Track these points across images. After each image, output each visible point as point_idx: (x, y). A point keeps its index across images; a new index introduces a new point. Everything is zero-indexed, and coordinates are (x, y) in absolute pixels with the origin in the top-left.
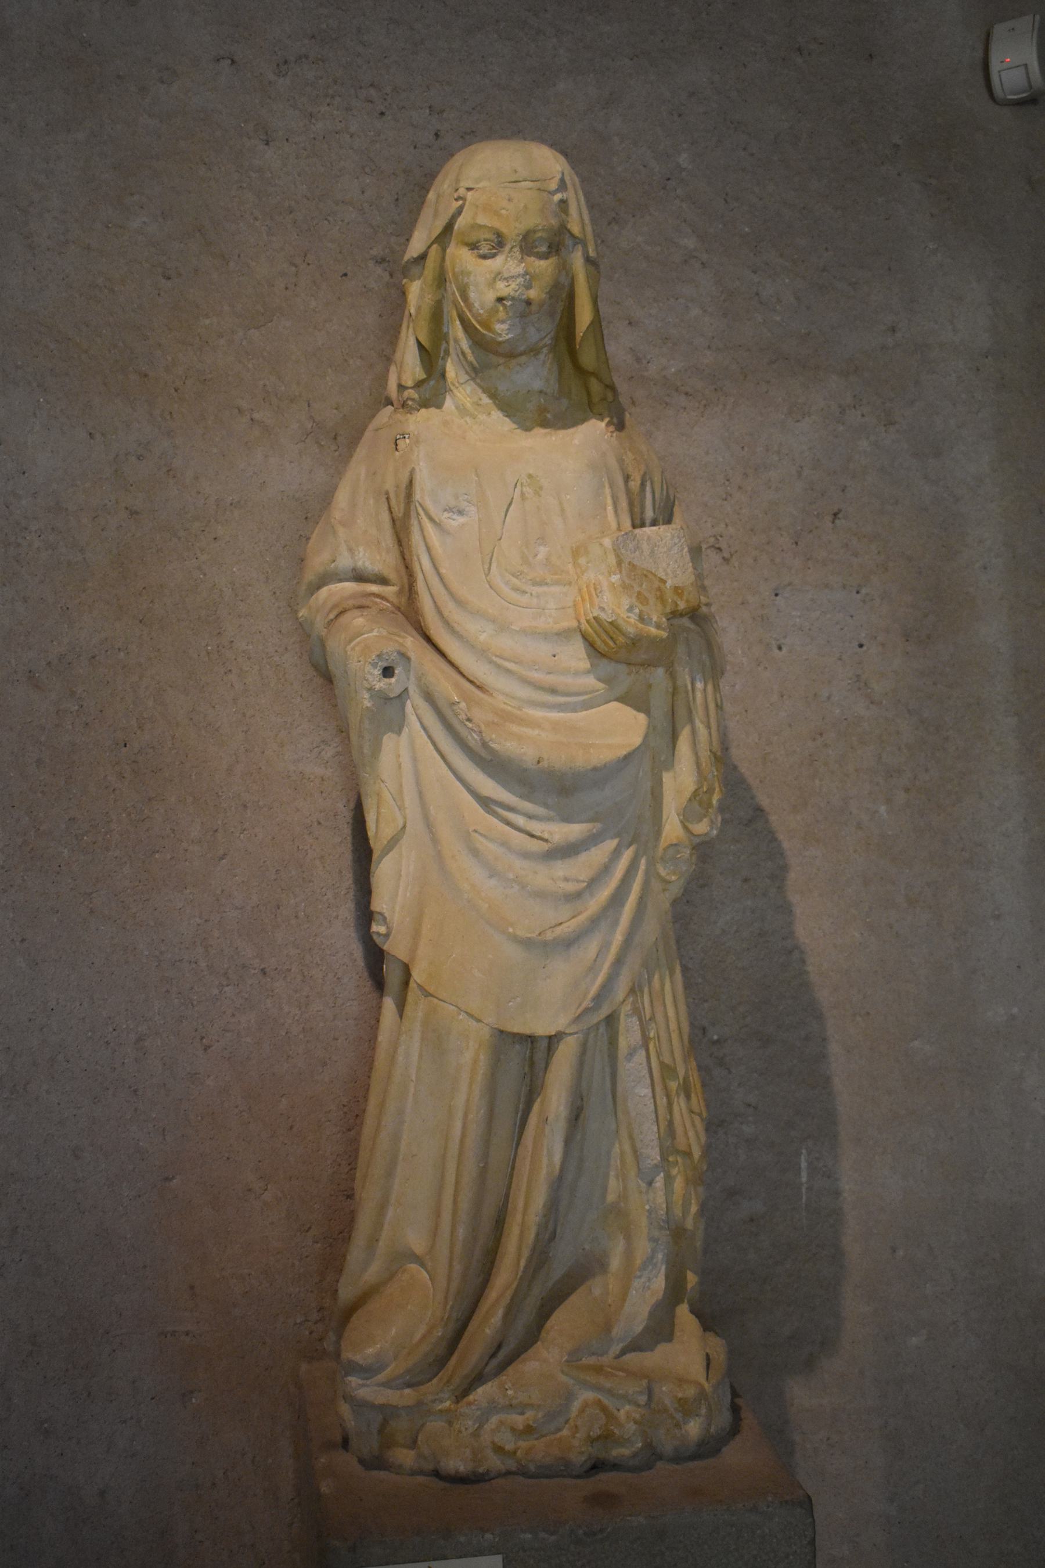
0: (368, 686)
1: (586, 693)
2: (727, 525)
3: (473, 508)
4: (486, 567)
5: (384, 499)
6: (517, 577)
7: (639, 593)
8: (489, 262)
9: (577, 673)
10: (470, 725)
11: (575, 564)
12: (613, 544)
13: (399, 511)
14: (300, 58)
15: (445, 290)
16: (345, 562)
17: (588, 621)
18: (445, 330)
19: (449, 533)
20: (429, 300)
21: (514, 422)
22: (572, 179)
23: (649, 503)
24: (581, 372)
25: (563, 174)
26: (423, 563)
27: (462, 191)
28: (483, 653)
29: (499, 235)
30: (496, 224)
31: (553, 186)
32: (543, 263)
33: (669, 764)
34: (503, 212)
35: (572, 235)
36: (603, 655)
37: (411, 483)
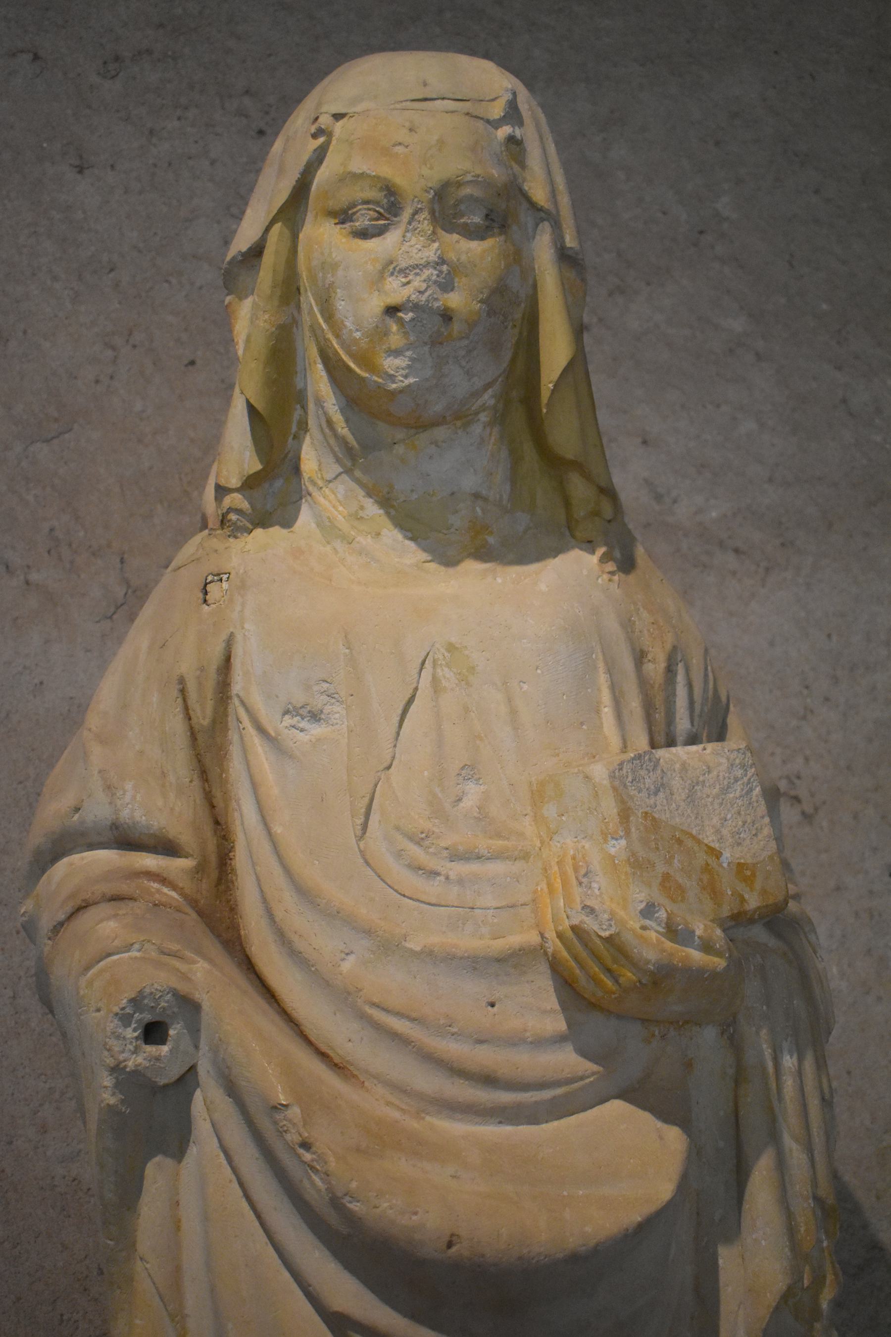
0: (110, 1062)
1: (557, 1084)
2: (807, 759)
3: (337, 708)
4: (360, 821)
5: (175, 693)
6: (419, 843)
7: (666, 877)
8: (372, 244)
9: (540, 1043)
10: (308, 1156)
11: (538, 819)
12: (612, 776)
13: (203, 716)
14: (140, 53)
15: (298, 307)
16: (98, 811)
17: (560, 936)
18: (300, 385)
19: (291, 757)
20: (266, 322)
21: (425, 550)
22: (530, 109)
23: (682, 708)
24: (554, 464)
25: (514, 94)
26: (245, 817)
27: (325, 121)
28: (345, 997)
29: (390, 190)
30: (386, 171)
31: (497, 111)
32: (476, 246)
33: (730, 1227)
34: (400, 149)
35: (533, 206)
36: (593, 1006)
37: (228, 660)
